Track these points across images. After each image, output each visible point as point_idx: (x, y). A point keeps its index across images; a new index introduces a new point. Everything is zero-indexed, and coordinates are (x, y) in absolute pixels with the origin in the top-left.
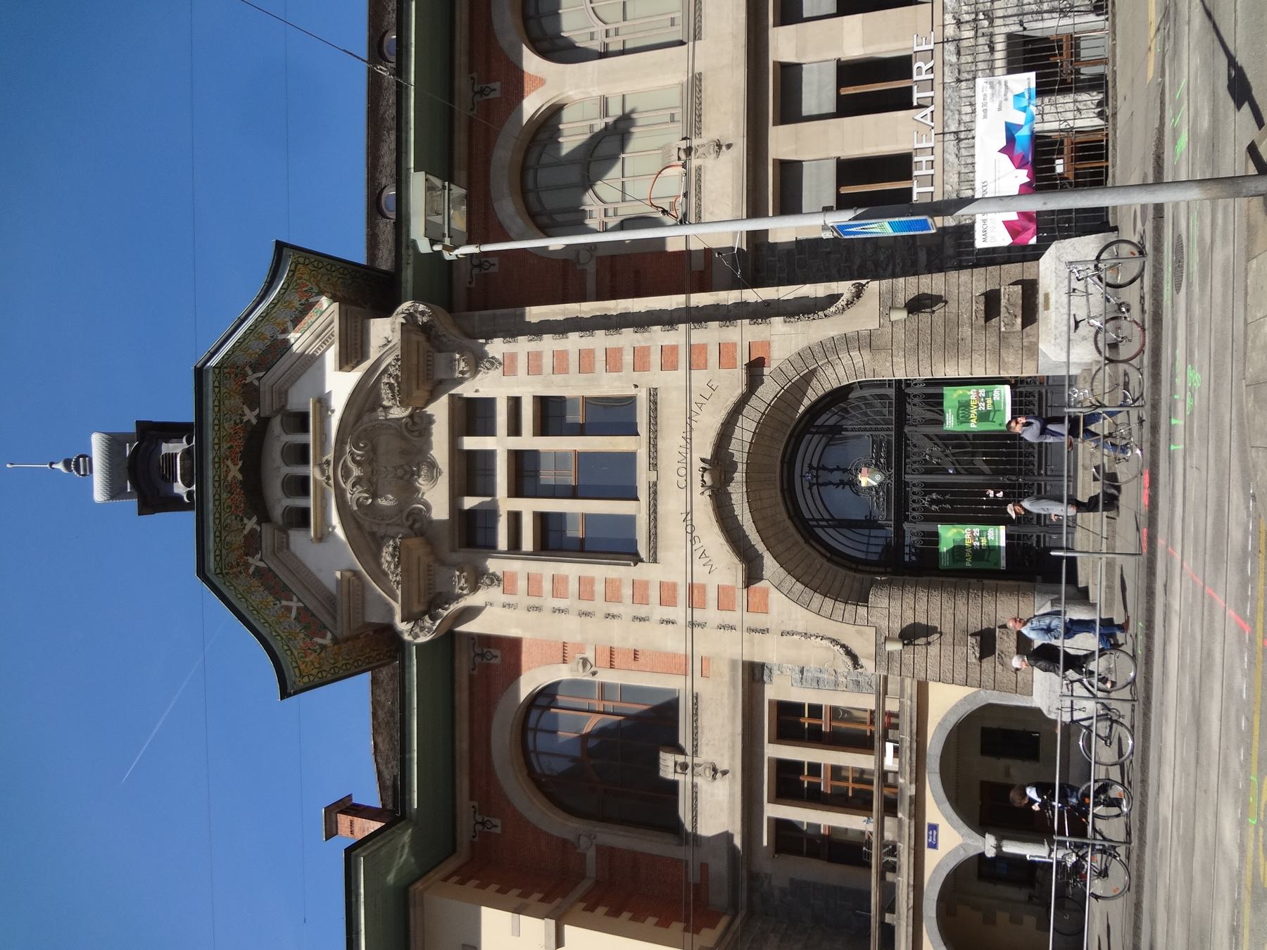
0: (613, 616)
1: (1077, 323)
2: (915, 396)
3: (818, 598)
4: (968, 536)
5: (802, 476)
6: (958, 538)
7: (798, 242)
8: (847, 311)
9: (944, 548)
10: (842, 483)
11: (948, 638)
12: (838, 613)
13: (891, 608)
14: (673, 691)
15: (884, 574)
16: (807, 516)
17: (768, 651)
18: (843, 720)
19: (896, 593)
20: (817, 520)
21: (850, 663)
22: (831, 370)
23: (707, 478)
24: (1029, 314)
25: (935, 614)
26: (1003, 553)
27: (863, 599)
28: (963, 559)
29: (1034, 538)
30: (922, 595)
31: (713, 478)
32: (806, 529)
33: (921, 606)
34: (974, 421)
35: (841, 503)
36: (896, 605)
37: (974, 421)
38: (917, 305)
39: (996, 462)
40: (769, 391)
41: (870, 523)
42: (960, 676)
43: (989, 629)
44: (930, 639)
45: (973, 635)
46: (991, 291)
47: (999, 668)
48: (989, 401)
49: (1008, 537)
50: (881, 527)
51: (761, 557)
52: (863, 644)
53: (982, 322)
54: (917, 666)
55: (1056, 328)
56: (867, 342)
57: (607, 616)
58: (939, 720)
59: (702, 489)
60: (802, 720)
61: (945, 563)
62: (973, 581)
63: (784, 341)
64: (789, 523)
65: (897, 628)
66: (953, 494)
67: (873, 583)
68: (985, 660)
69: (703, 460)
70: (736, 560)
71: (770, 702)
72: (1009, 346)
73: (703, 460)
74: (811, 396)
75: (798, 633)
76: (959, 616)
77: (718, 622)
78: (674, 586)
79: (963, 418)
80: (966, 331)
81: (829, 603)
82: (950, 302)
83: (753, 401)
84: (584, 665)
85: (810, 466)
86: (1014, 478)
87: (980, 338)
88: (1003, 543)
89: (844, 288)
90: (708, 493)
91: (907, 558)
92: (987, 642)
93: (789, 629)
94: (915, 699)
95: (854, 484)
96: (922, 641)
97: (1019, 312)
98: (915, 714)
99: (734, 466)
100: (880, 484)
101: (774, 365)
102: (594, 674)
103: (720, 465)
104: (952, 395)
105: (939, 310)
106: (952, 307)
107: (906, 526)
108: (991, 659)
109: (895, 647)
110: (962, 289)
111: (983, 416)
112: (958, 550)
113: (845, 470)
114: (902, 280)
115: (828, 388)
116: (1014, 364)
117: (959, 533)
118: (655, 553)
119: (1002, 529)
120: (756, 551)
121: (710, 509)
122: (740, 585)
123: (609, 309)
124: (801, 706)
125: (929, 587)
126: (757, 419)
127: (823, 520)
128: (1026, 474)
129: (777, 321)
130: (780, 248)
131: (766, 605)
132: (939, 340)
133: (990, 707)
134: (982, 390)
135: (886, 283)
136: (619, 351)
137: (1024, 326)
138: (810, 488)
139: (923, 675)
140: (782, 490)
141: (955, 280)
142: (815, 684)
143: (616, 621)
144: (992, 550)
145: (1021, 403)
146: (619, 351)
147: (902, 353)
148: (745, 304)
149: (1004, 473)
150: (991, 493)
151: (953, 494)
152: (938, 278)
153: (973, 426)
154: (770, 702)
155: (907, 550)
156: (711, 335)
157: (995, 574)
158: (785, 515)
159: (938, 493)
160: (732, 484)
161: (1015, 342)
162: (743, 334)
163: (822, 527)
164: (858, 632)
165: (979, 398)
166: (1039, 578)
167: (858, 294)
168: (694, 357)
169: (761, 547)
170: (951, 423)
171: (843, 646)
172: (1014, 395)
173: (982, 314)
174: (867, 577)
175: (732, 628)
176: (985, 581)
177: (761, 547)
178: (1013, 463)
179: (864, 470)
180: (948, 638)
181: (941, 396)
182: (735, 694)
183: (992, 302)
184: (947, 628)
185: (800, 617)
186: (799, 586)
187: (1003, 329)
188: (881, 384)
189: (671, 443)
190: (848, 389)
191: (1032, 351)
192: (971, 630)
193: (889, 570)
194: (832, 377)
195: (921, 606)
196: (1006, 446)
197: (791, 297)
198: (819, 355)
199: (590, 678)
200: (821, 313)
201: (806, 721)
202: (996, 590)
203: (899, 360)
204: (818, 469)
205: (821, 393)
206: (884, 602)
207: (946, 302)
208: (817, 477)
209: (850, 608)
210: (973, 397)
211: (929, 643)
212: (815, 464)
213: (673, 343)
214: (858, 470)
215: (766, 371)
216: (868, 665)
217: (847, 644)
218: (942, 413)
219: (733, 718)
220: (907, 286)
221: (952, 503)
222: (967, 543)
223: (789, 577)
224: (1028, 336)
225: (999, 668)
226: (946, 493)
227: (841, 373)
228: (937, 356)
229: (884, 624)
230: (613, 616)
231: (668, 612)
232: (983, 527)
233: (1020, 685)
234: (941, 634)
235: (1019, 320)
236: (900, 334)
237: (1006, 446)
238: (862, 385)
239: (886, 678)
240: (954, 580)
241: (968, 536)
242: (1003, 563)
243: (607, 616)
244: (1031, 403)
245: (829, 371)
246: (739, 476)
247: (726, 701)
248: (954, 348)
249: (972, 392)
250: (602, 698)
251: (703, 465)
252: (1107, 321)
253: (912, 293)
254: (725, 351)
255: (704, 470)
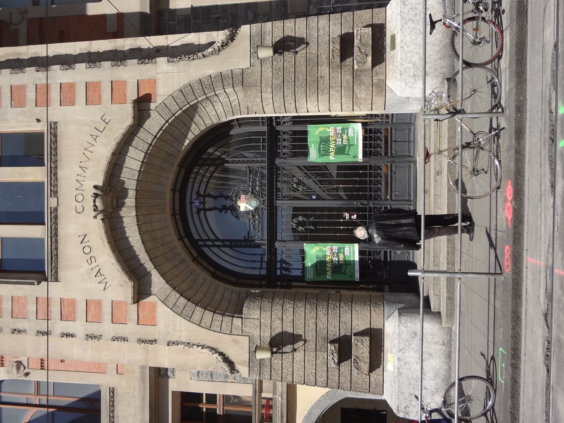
0: (19, 331)
1: (433, 24)
2: (284, 133)
3: (199, 311)
4: (328, 253)
5: (191, 203)
6: (321, 254)
7: (193, 9)
8: (223, 53)
9: (309, 263)
10: (224, 209)
11: (311, 345)
12: (217, 324)
13: (263, 318)
14: (98, 386)
15: (260, 286)
16: (196, 237)
17: (163, 358)
18: (233, 404)
19: (267, 305)
20: (204, 241)
21: (227, 369)
22: (211, 107)
23: (99, 203)
24: (378, 55)
25: (300, 324)
26: (357, 267)
27: (238, 311)
28: (325, 273)
29: (382, 253)
30: (289, 306)
31: (104, 203)
32: (198, 250)
33: (288, 316)
34: (332, 154)
35: (216, 224)
36: (266, 315)
37: (332, 154)
38: (283, 46)
39: (351, 190)
40: (154, 124)
41: (248, 242)
42: (322, 379)
43: (345, 336)
44: (296, 346)
45: (332, 342)
46: (346, 34)
47: (355, 371)
48: (345, 137)
49: (361, 253)
50: (258, 246)
51: (149, 274)
52: (238, 351)
53: (338, 60)
54: (285, 371)
55: (401, 65)
56: (239, 79)
57: (14, 331)
58: (305, 413)
59: (94, 214)
60: (201, 406)
61: (310, 276)
62: (333, 292)
63: (168, 79)
64: (178, 245)
65: (267, 336)
66: (315, 216)
67: (249, 296)
68: (342, 364)
69: (96, 187)
70: (125, 278)
71: (173, 392)
72: (361, 83)
73: (96, 187)
74: (194, 132)
75: (183, 343)
76: (320, 325)
77: (112, 334)
78: (73, 302)
79: (324, 152)
80: (324, 70)
81: (208, 315)
82: (311, 44)
83: (141, 134)
84: (18, 368)
85: (198, 194)
86: (365, 202)
87: (336, 75)
88: (357, 258)
89: (219, 36)
90: (100, 216)
91: (278, 272)
92: (344, 348)
93: (174, 339)
94: (285, 397)
95: (234, 209)
96: (288, 348)
97: (370, 52)
98: (285, 409)
99: (124, 193)
100: (256, 209)
101: (159, 100)
102: (27, 374)
103: (110, 193)
104: (315, 132)
105: (301, 50)
106: (312, 48)
107: (277, 244)
108: (347, 363)
109: (264, 355)
110: (321, 32)
111: (340, 150)
112: (321, 265)
113: (227, 197)
114: (269, 24)
115: (209, 123)
116: (365, 100)
117: (321, 250)
118: (56, 272)
119: (356, 246)
120: (145, 269)
121: (102, 231)
122: (130, 300)
123: (20, 54)
124: (200, 395)
125: (295, 298)
126: (145, 149)
127: (209, 240)
128: (375, 199)
129: (162, 61)
130: (178, 13)
131: (154, 318)
132: (301, 77)
133: (347, 400)
134: (339, 127)
135: (256, 27)
136: (23, 88)
137: (374, 64)
138: (198, 213)
139: (290, 379)
140: (174, 215)
141: (315, 24)
142: (209, 377)
143: (22, 335)
144: (348, 264)
145: (371, 138)
146: (23, 88)
147: (269, 90)
148: (139, 50)
149: (358, 198)
150: (347, 215)
151: (315, 216)
152: (301, 22)
153: (332, 158)
154: (173, 392)
155: (278, 265)
156: (105, 73)
157: (351, 285)
158: (174, 237)
159: (304, 216)
160: (124, 209)
161: (366, 79)
162: (131, 73)
163: (209, 247)
164: (234, 341)
165: (336, 134)
166: (386, 287)
167: (232, 38)
168: (89, 93)
169: (149, 266)
170: (314, 156)
171: (221, 354)
172: (366, 131)
173: (337, 53)
174: (243, 290)
175: (125, 339)
176: (343, 292)
177: (149, 266)
178: (365, 190)
179: (243, 197)
180: (311, 345)
181: (305, 133)
182: (144, 388)
183: (346, 44)
184: (310, 336)
185: (183, 329)
186: (183, 300)
187: (356, 67)
188: (255, 121)
189: (68, 173)
190: (229, 125)
191: (381, 87)
192: (331, 338)
193: (264, 283)
194: (212, 115)
195: (288, 316)
196: (359, 175)
197: (178, 44)
198: (198, 92)
199: (24, 378)
200: (200, 54)
201: (204, 407)
202: (352, 301)
203: (267, 95)
204: (204, 196)
205: (203, 128)
206: (256, 314)
207: (307, 44)
208: (204, 203)
209: (227, 319)
210: (332, 134)
211: (295, 350)
212: (202, 192)
213: (71, 81)
214: (238, 197)
215: (153, 106)
216: (243, 370)
217: (224, 352)
218: (306, 147)
219: (143, 409)
220: (275, 30)
221: (314, 224)
222: (328, 259)
223: (174, 293)
224: (377, 74)
225: (355, 371)
226: (311, 216)
227: (220, 110)
228: (300, 92)
229: (256, 333)
230: (19, 331)
231: (67, 326)
232: (341, 245)
233: (373, 385)
234: (305, 341)
235: (370, 59)
236: (268, 73)
237: (359, 175)
238: (240, 122)
239: (261, 382)
240: (316, 291)
241: (328, 253)
242: (357, 275)
243: (14, 331)
244: (379, 139)
245: (209, 108)
246: (130, 201)
247: (137, 394)
248: (314, 85)
249: (331, 129)
250: (38, 393)
251: (95, 191)
252: (464, 22)
253: (278, 36)
254: (117, 89)
255: (96, 195)
